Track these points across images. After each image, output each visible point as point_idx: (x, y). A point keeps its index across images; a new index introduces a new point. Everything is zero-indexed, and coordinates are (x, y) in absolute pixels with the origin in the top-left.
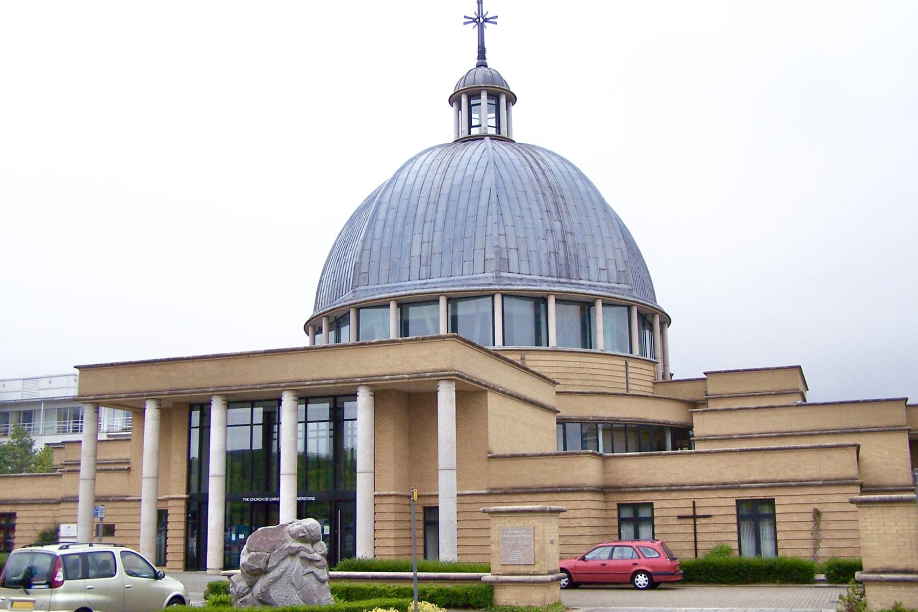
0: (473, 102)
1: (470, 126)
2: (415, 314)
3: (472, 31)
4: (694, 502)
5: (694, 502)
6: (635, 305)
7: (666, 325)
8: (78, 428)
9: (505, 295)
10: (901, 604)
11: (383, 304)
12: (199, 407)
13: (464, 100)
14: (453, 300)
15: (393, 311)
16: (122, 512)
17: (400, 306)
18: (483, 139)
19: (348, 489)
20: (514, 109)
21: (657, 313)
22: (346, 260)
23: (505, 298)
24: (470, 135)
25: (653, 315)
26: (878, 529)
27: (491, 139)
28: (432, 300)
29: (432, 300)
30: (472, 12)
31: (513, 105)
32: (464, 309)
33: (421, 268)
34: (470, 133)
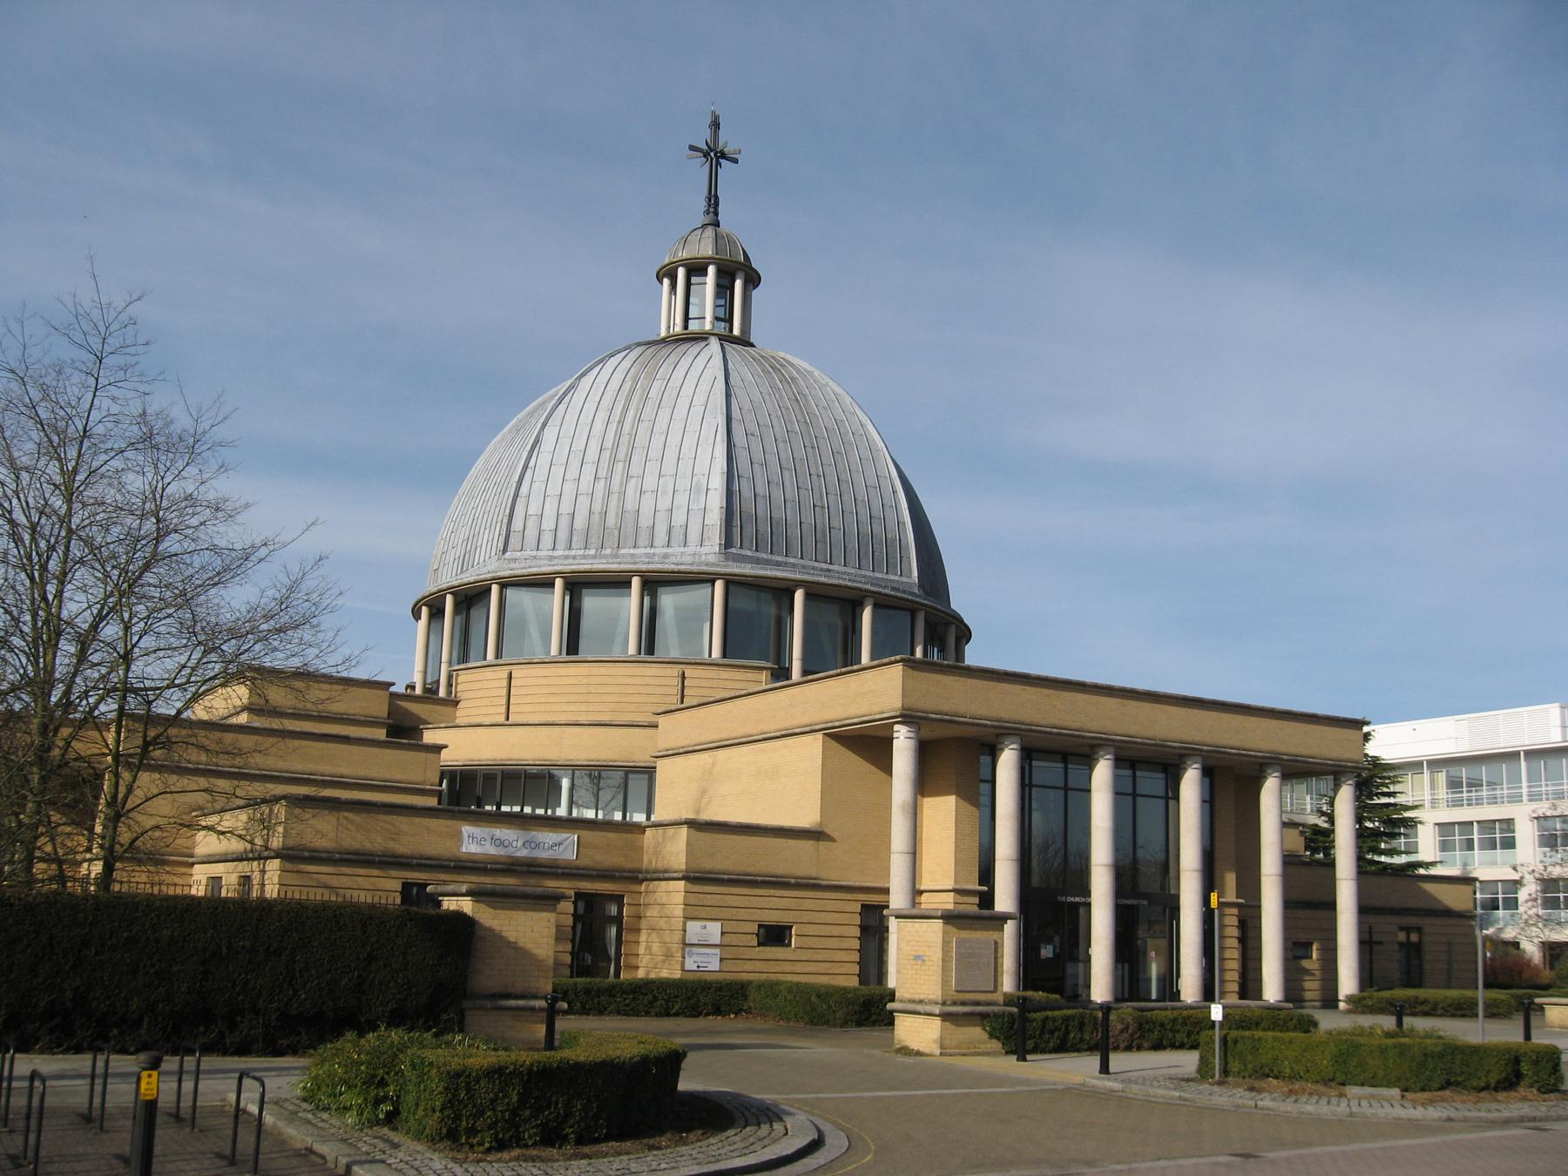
0: (694, 280)
1: (686, 319)
2: (592, 603)
3: (700, 169)
4: (1370, 927)
5: (1370, 927)
6: (922, 610)
7: (964, 640)
8: (1463, 800)
9: (732, 582)
10: (1018, 1060)
11: (543, 583)
12: (1060, 757)
13: (681, 272)
14: (653, 583)
15: (557, 598)
16: (807, 904)
17: (570, 587)
18: (706, 339)
19: (1172, 892)
20: (756, 294)
21: (953, 623)
22: (477, 515)
23: (731, 587)
24: (686, 331)
25: (947, 625)
26: (502, 925)
27: (720, 340)
28: (618, 582)
29: (618, 582)
30: (702, 138)
31: (754, 289)
32: (669, 600)
33: (554, 528)
34: (686, 327)
